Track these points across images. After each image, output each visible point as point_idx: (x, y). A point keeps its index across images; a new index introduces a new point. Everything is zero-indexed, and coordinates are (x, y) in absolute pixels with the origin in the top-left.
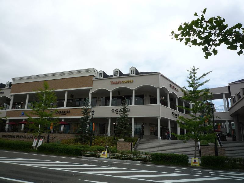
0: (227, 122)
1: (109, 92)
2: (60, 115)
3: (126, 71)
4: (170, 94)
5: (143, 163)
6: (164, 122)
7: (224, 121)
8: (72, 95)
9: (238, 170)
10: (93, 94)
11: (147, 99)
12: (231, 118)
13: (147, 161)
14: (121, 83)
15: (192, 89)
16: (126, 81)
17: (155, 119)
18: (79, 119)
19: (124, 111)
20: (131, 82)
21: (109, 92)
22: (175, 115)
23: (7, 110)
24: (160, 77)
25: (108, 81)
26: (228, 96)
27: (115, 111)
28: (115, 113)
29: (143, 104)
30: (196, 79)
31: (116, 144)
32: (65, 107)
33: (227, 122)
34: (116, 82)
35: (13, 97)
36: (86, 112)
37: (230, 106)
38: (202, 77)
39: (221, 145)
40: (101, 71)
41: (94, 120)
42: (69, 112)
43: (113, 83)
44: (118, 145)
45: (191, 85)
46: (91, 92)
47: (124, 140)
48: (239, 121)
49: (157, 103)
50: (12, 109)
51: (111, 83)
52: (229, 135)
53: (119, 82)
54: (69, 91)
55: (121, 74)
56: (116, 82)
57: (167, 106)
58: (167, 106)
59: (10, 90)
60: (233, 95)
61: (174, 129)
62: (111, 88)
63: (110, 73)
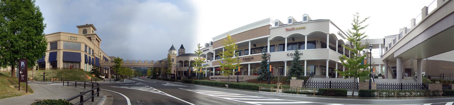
0: (380, 65)
1: (285, 39)
2: (246, 61)
3: (299, 19)
4: (338, 41)
5: (309, 96)
6: (332, 64)
7: (378, 65)
8: (254, 43)
9: (446, 97)
10: (271, 41)
11: (318, 45)
12: (383, 63)
13: (313, 94)
14: (294, 30)
15: (355, 31)
16: (299, 27)
17: (324, 61)
18: (260, 63)
19: (297, 54)
20: (304, 28)
21: (285, 39)
22: (342, 59)
23: (212, 61)
24: (330, 24)
25: (284, 29)
26: (383, 46)
27: (290, 55)
28: (290, 56)
29: (315, 48)
30: (359, 22)
31: (290, 82)
32: (250, 55)
33: (380, 65)
34: (290, 29)
35: (214, 51)
36: (265, 57)
37: (383, 54)
38: (364, 21)
39: (374, 81)
40: (276, 20)
41: (273, 64)
42: (253, 58)
43: (287, 30)
44: (291, 82)
45: (355, 28)
46: (269, 40)
47: (296, 78)
48: (388, 65)
49: (326, 47)
50: (215, 60)
51: (286, 30)
52: (380, 75)
53: (293, 29)
54: (251, 41)
55: (296, 23)
56: (290, 29)
57: (335, 51)
58: (335, 51)
59: (212, 47)
60: (386, 45)
61: (340, 70)
62: (286, 35)
63: (285, 22)
